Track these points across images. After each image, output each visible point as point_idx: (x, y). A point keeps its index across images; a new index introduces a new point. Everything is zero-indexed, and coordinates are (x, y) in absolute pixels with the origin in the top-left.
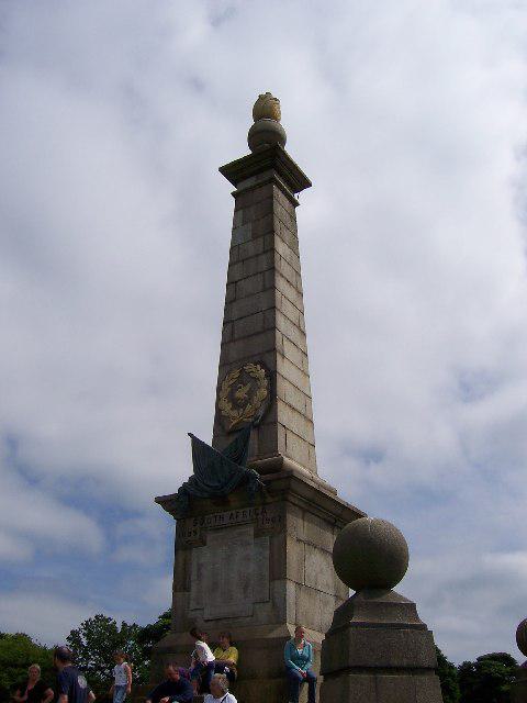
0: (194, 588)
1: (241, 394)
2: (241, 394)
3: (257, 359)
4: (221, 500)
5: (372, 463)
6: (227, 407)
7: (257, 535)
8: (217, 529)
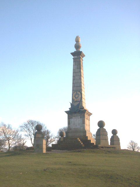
0: (71, 124)
1: (77, 96)
2: (77, 96)
3: (79, 91)
4: (75, 113)
5: (42, 131)
6: (74, 98)
7: (80, 118)
8: (74, 116)
